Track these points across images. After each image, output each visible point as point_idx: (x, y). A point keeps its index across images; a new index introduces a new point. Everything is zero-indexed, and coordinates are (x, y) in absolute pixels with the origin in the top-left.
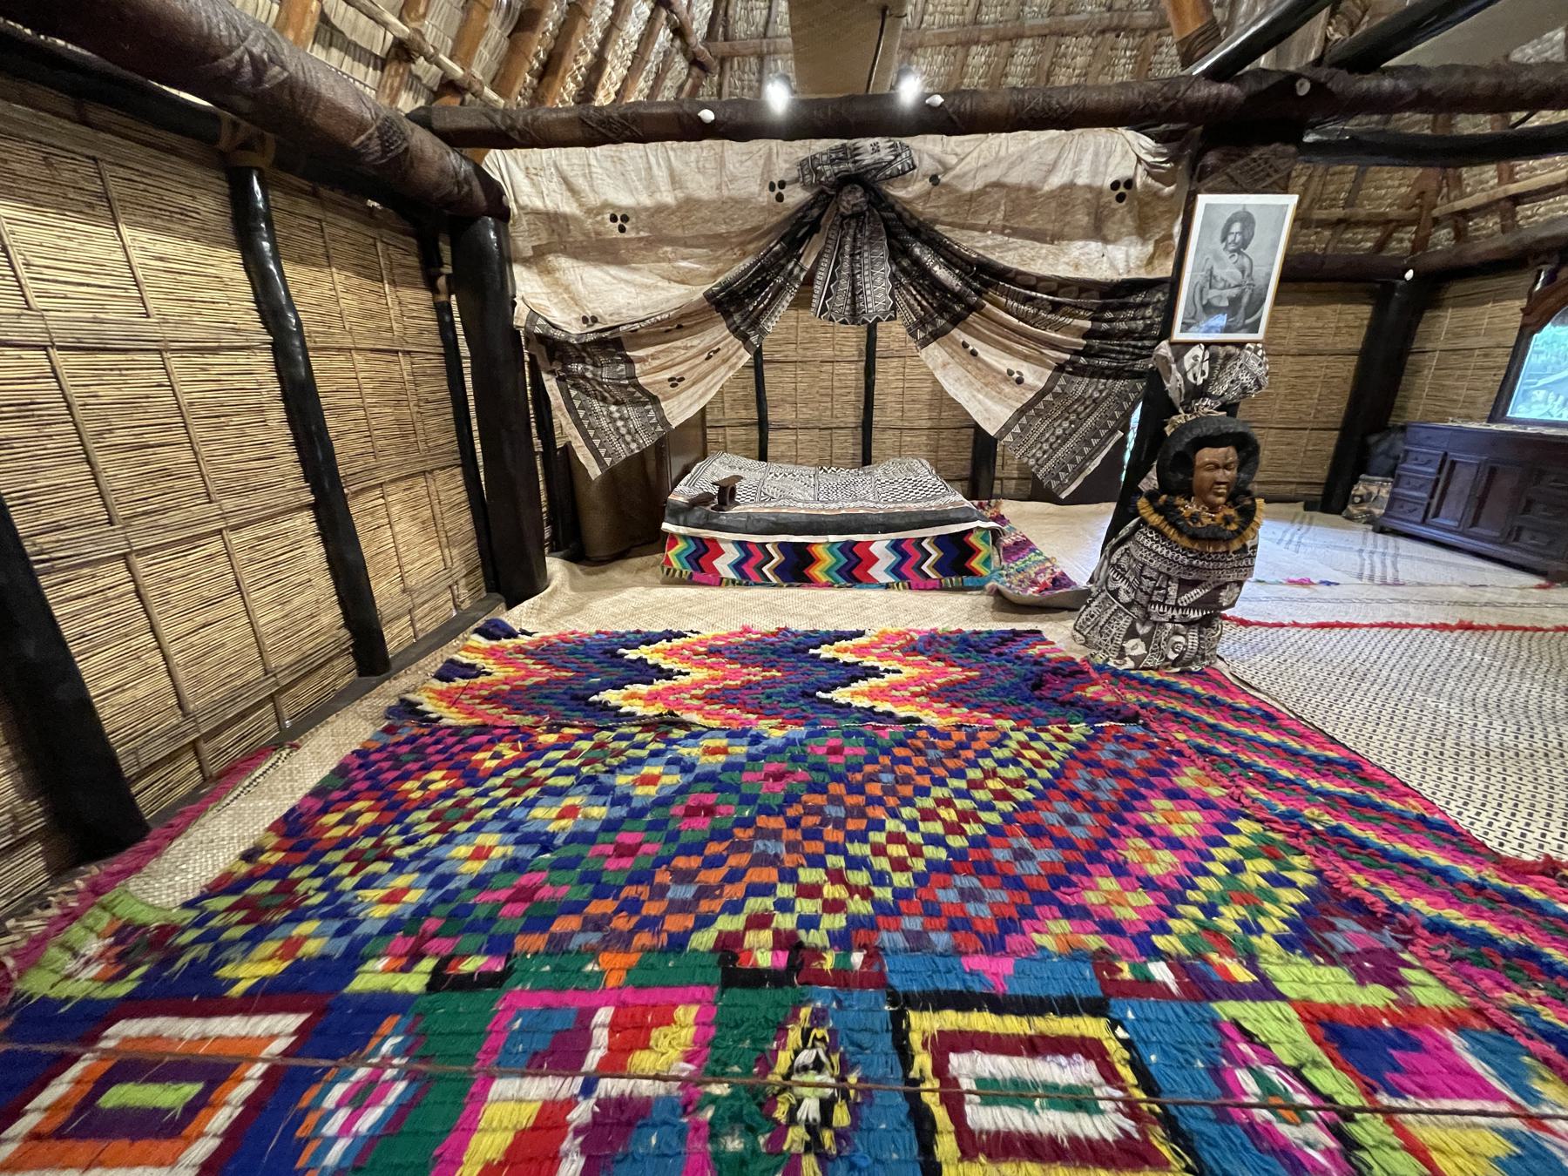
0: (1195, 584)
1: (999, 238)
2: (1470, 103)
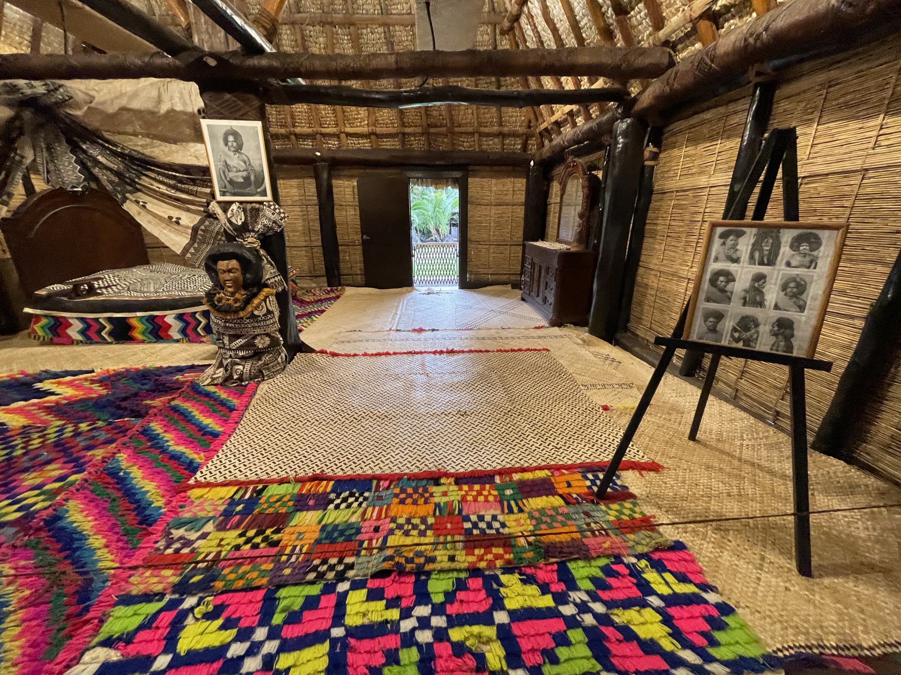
0: (238, 337)
1: (148, 140)
2: (356, 74)
